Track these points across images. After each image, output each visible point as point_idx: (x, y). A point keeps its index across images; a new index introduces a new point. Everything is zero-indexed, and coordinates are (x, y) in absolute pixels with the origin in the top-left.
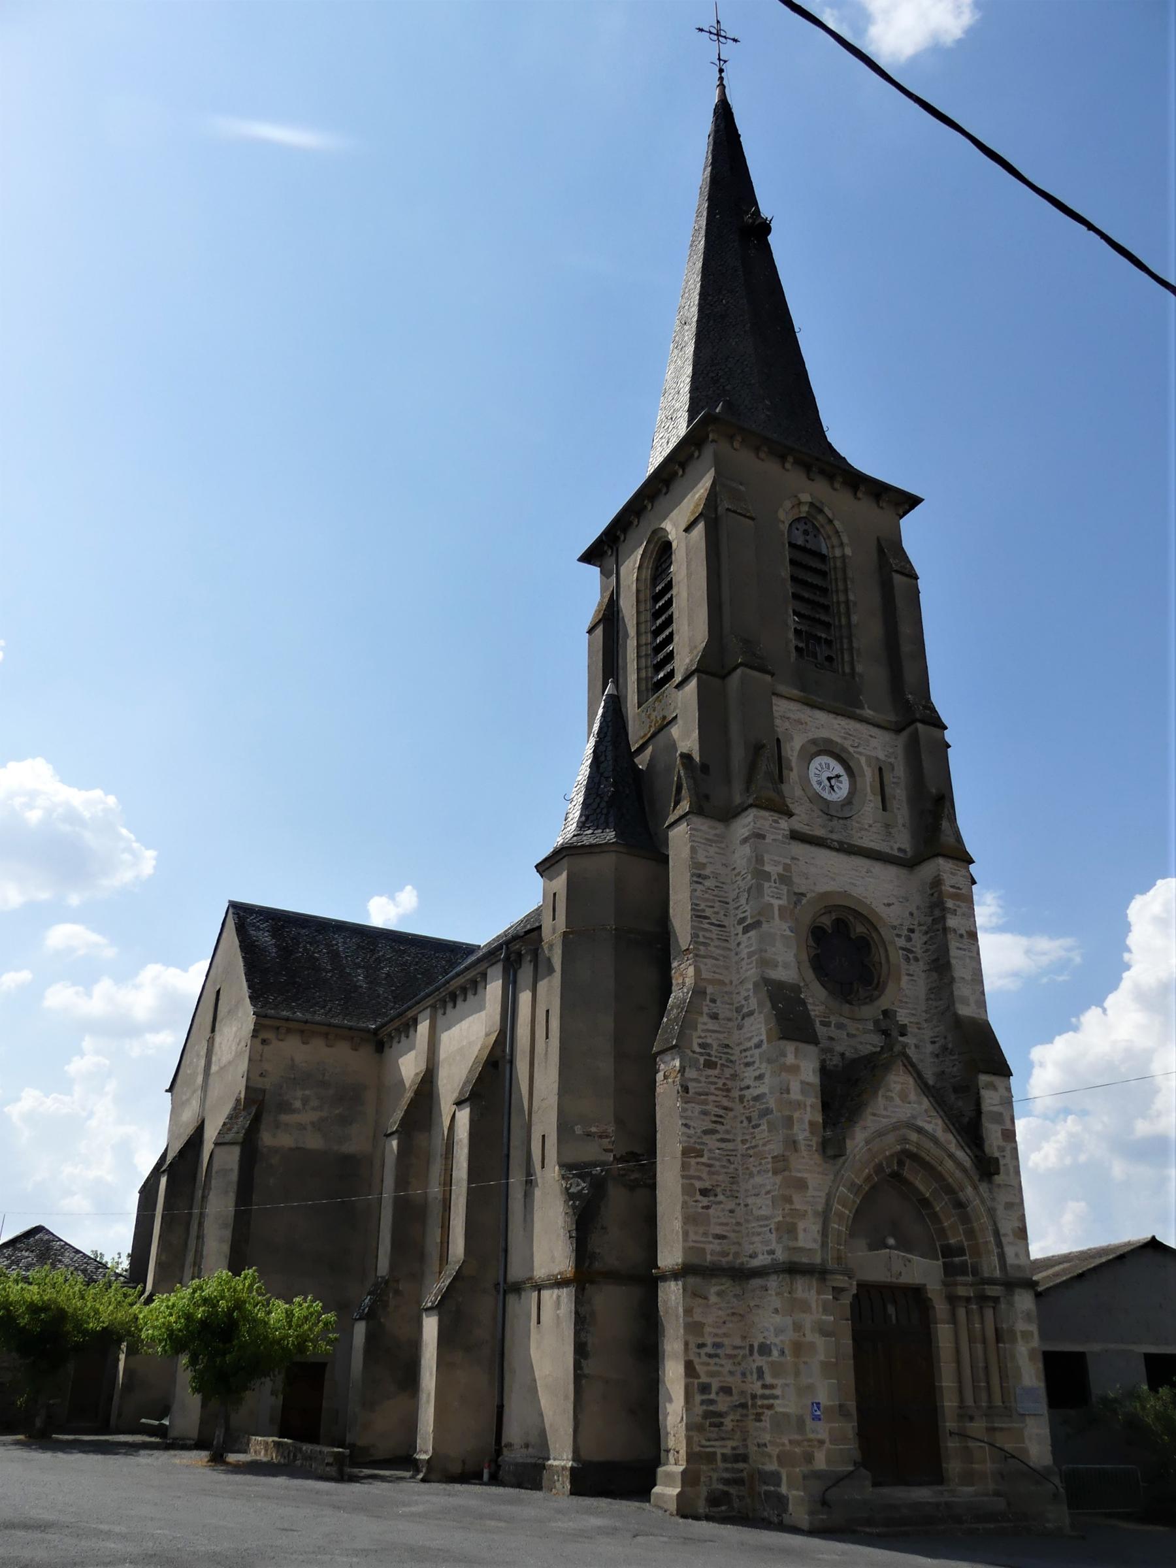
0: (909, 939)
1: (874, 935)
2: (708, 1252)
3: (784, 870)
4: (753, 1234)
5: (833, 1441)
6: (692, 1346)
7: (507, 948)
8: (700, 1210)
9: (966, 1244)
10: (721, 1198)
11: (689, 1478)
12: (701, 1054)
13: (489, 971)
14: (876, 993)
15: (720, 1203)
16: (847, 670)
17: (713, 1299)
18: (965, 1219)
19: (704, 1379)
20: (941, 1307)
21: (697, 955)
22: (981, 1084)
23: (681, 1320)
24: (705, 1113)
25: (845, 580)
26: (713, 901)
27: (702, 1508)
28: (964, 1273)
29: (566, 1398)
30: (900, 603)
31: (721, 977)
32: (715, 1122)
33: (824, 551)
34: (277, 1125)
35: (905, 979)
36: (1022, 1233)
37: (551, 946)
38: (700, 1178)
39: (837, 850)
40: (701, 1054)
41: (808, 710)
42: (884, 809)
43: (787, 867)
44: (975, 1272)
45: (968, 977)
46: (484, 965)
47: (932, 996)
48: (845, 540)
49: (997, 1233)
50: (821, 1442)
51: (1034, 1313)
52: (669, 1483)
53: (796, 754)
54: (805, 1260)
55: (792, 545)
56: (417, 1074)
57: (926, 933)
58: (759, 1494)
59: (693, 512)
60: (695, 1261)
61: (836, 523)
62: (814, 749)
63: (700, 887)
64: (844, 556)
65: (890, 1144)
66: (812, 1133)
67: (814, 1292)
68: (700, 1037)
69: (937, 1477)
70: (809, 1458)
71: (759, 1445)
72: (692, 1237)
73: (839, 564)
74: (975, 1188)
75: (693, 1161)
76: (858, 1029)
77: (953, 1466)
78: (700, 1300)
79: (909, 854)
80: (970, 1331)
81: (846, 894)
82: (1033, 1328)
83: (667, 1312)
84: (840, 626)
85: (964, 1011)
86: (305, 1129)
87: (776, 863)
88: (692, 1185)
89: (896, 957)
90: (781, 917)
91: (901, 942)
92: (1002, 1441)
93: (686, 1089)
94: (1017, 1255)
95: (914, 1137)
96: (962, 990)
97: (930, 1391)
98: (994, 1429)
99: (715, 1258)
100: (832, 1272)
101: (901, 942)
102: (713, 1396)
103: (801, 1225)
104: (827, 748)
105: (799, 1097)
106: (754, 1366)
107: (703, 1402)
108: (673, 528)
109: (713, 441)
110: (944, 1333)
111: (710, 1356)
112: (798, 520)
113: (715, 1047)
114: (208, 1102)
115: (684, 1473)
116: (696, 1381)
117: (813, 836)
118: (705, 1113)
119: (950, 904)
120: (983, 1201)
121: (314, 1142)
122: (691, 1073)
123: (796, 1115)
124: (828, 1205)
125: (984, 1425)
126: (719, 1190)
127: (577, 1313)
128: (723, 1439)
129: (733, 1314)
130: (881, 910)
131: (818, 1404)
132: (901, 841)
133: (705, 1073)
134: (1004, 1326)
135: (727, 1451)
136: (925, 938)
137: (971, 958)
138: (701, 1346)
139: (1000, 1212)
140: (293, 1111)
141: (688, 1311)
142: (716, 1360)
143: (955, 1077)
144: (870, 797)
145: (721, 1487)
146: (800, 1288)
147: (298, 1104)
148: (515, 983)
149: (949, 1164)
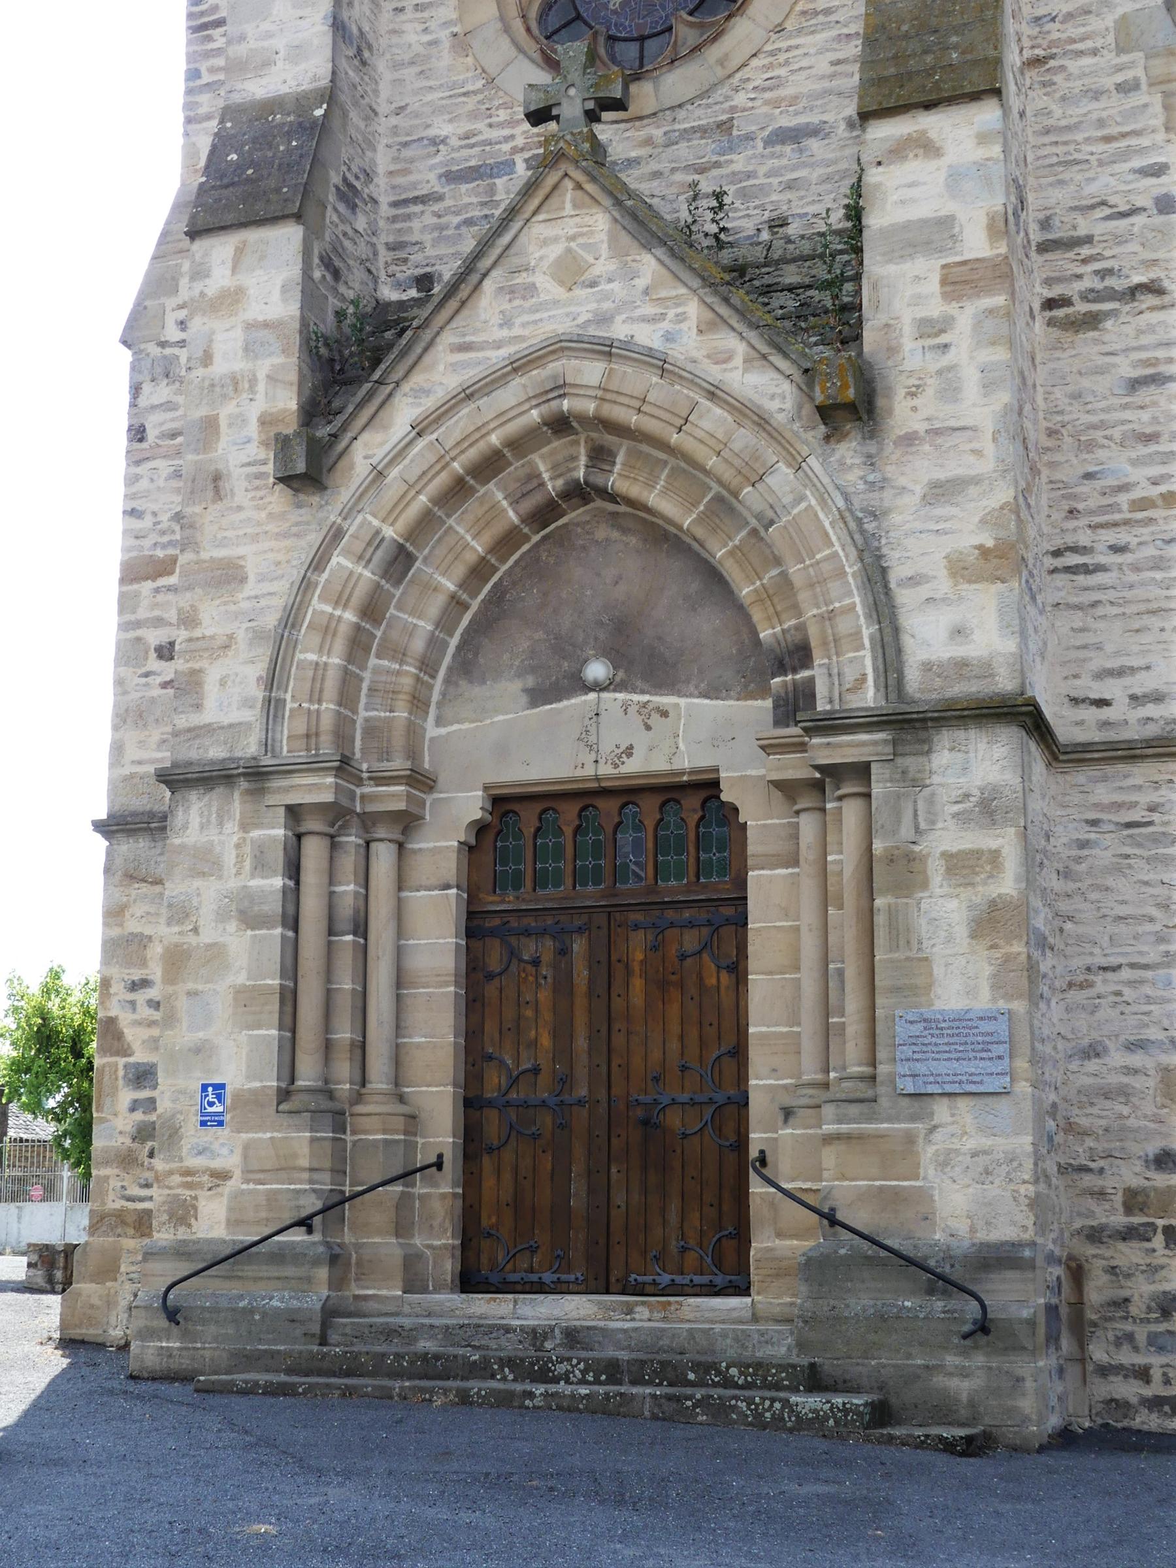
5: (249, 1174)
6: (117, 988)
19: (140, 1056)
20: (761, 821)
50: (222, 1176)
54: (216, 752)
65: (513, 407)
67: (231, 827)
70: (183, 1213)
78: (145, 888)
95: (591, 372)
100: (286, 771)
103: (213, 675)
105: (239, 365)
107: (134, 1106)
116: (122, 1061)
123: (226, 411)
138: (136, 986)
146: (195, 819)
149: (713, 419)
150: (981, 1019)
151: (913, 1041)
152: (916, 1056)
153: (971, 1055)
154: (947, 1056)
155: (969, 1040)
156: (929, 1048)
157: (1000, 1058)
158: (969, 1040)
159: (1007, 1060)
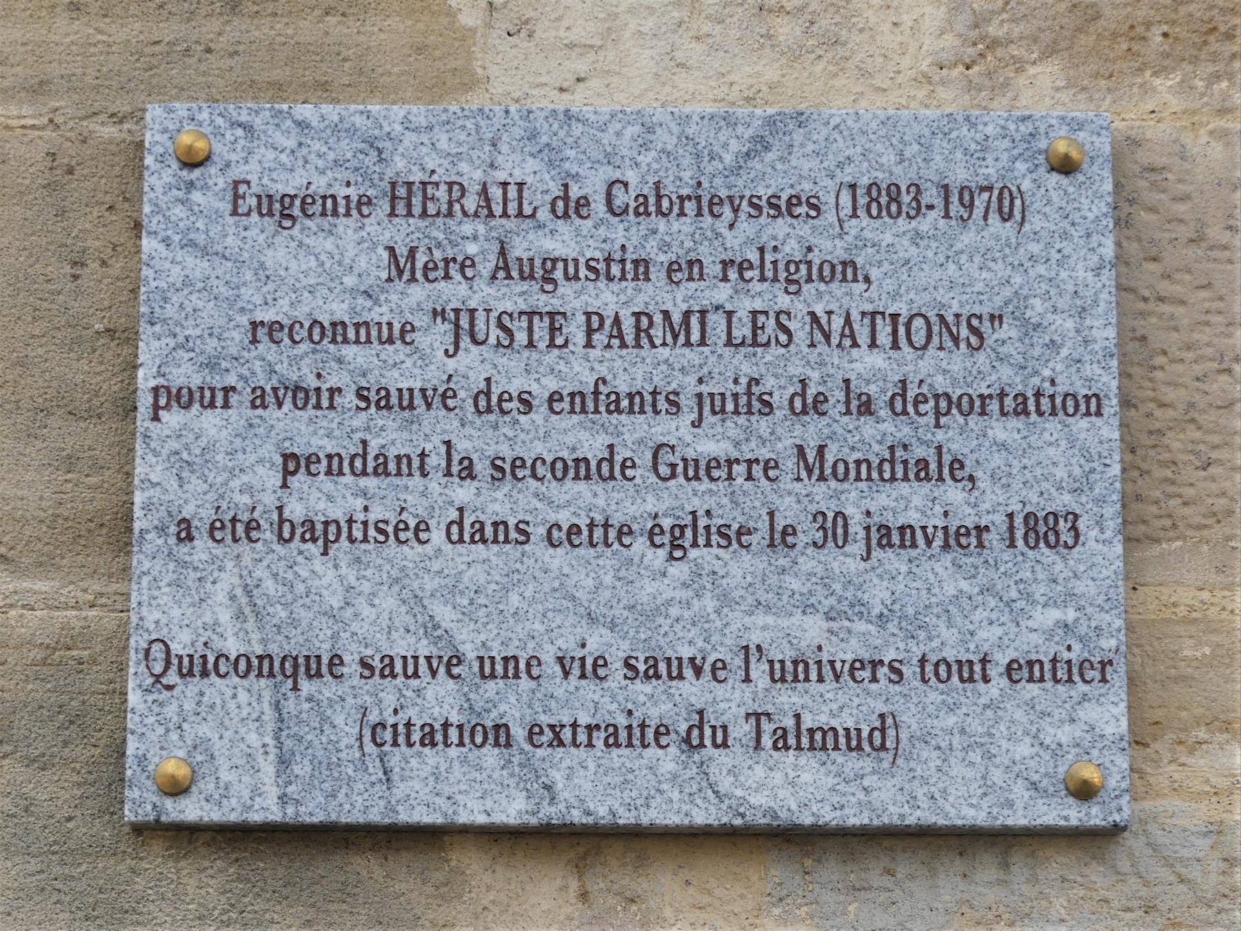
150: (885, 200)
151: (291, 363)
152: (314, 498)
153: (795, 500)
154: (577, 500)
155: (779, 371)
156: (432, 431)
157: (1044, 530)
158: (779, 371)
159: (1102, 551)
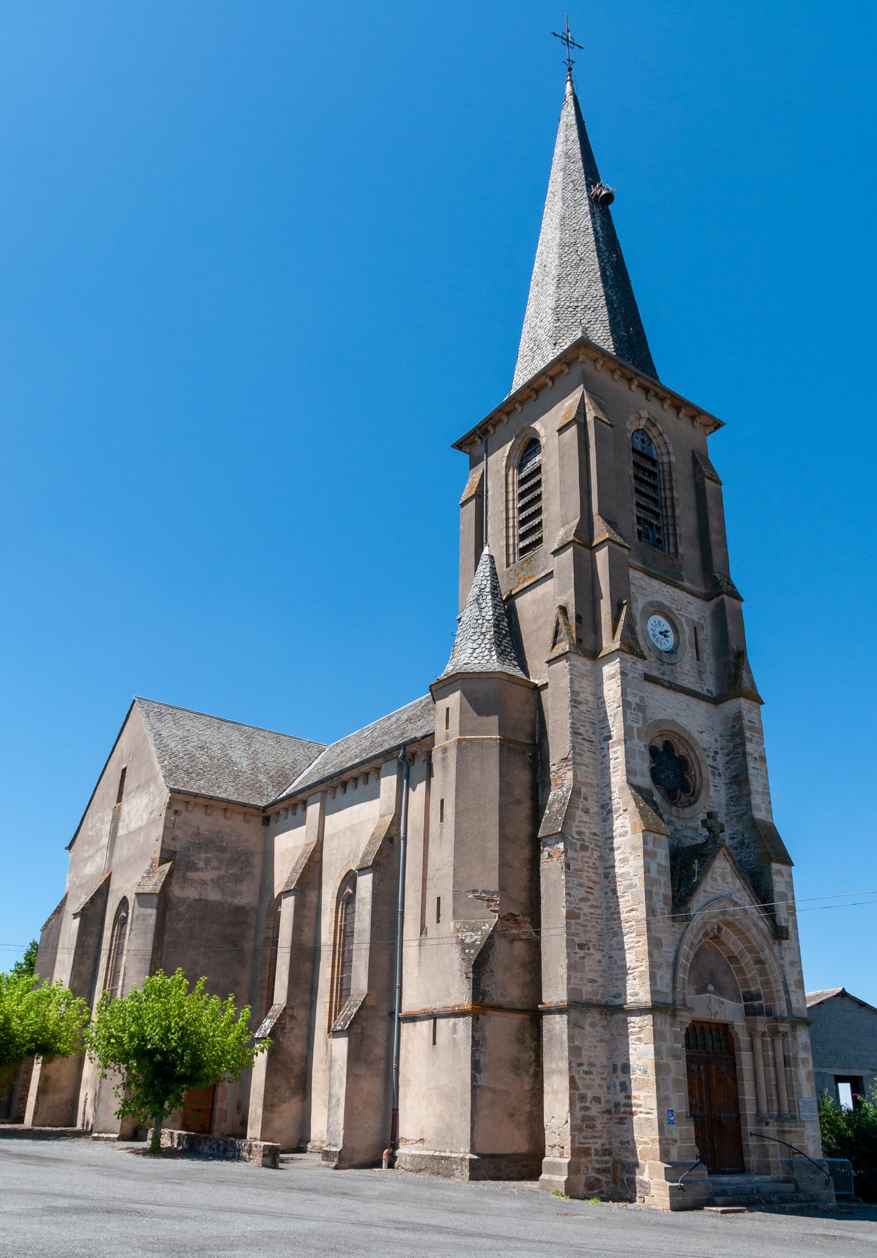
0: (714, 760)
1: (691, 755)
2: (584, 992)
3: (641, 701)
4: (617, 979)
6: (574, 1065)
7: (405, 749)
8: (578, 960)
9: (762, 991)
10: (592, 950)
11: (573, 1168)
12: (578, 840)
13: (383, 766)
14: (693, 798)
15: (592, 954)
16: (672, 550)
17: (588, 1028)
18: (763, 972)
19: (582, 1091)
20: (743, 1039)
21: (574, 763)
22: (773, 871)
23: (566, 1045)
24: (581, 885)
25: (671, 481)
26: (585, 721)
27: (582, 1189)
28: (761, 1014)
29: (463, 1104)
30: (710, 502)
31: (591, 781)
32: (588, 892)
33: (655, 458)
34: (185, 880)
35: (712, 789)
36: (800, 984)
37: (445, 750)
38: (577, 935)
39: (668, 688)
40: (578, 840)
41: (646, 578)
42: (698, 660)
43: (642, 699)
44: (769, 1013)
45: (760, 790)
46: (381, 760)
47: (732, 803)
48: (671, 450)
49: (785, 985)
51: (809, 1045)
52: (555, 1168)
53: (639, 612)
55: (635, 451)
56: (307, 845)
57: (728, 755)
58: (622, 1180)
59: (565, 417)
60: (577, 999)
61: (665, 436)
62: (652, 609)
63: (576, 710)
64: (670, 462)
66: (665, 903)
67: (667, 1026)
68: (577, 826)
69: (742, 1169)
71: (622, 1143)
72: (573, 980)
73: (666, 468)
74: (771, 949)
75: (573, 921)
76: (682, 826)
77: (753, 1160)
79: (714, 695)
80: (765, 1058)
81: (672, 722)
82: (809, 1056)
83: (551, 1038)
84: (667, 516)
85: (759, 815)
86: (207, 884)
87: (635, 695)
88: (573, 940)
89: (707, 773)
90: (639, 737)
91: (710, 761)
92: (790, 1139)
93: (568, 866)
94: (798, 1001)
96: (756, 800)
97: (736, 1103)
98: (784, 1132)
99: (589, 997)
101: (710, 761)
102: (588, 1104)
104: (660, 609)
106: (618, 1083)
108: (545, 427)
109: (583, 362)
110: (745, 1058)
111: (586, 1073)
112: (638, 430)
113: (588, 835)
114: (115, 860)
115: (569, 1164)
117: (652, 676)
118: (581, 885)
119: (748, 734)
120: (776, 960)
121: (214, 895)
122: (571, 853)
124: (676, 958)
125: (776, 1128)
126: (591, 944)
127: (473, 1037)
128: (595, 1137)
129: (602, 1040)
130: (696, 735)
131: (672, 1111)
132: (709, 685)
133: (580, 855)
134: (791, 1054)
135: (598, 1146)
136: (727, 759)
137: (762, 775)
138: (580, 1065)
139: (787, 968)
140: (197, 870)
141: (571, 1038)
142: (590, 1076)
143: (750, 865)
144: (688, 649)
145: (594, 1174)
147: (201, 864)
148: (408, 777)
149: (754, 931)
